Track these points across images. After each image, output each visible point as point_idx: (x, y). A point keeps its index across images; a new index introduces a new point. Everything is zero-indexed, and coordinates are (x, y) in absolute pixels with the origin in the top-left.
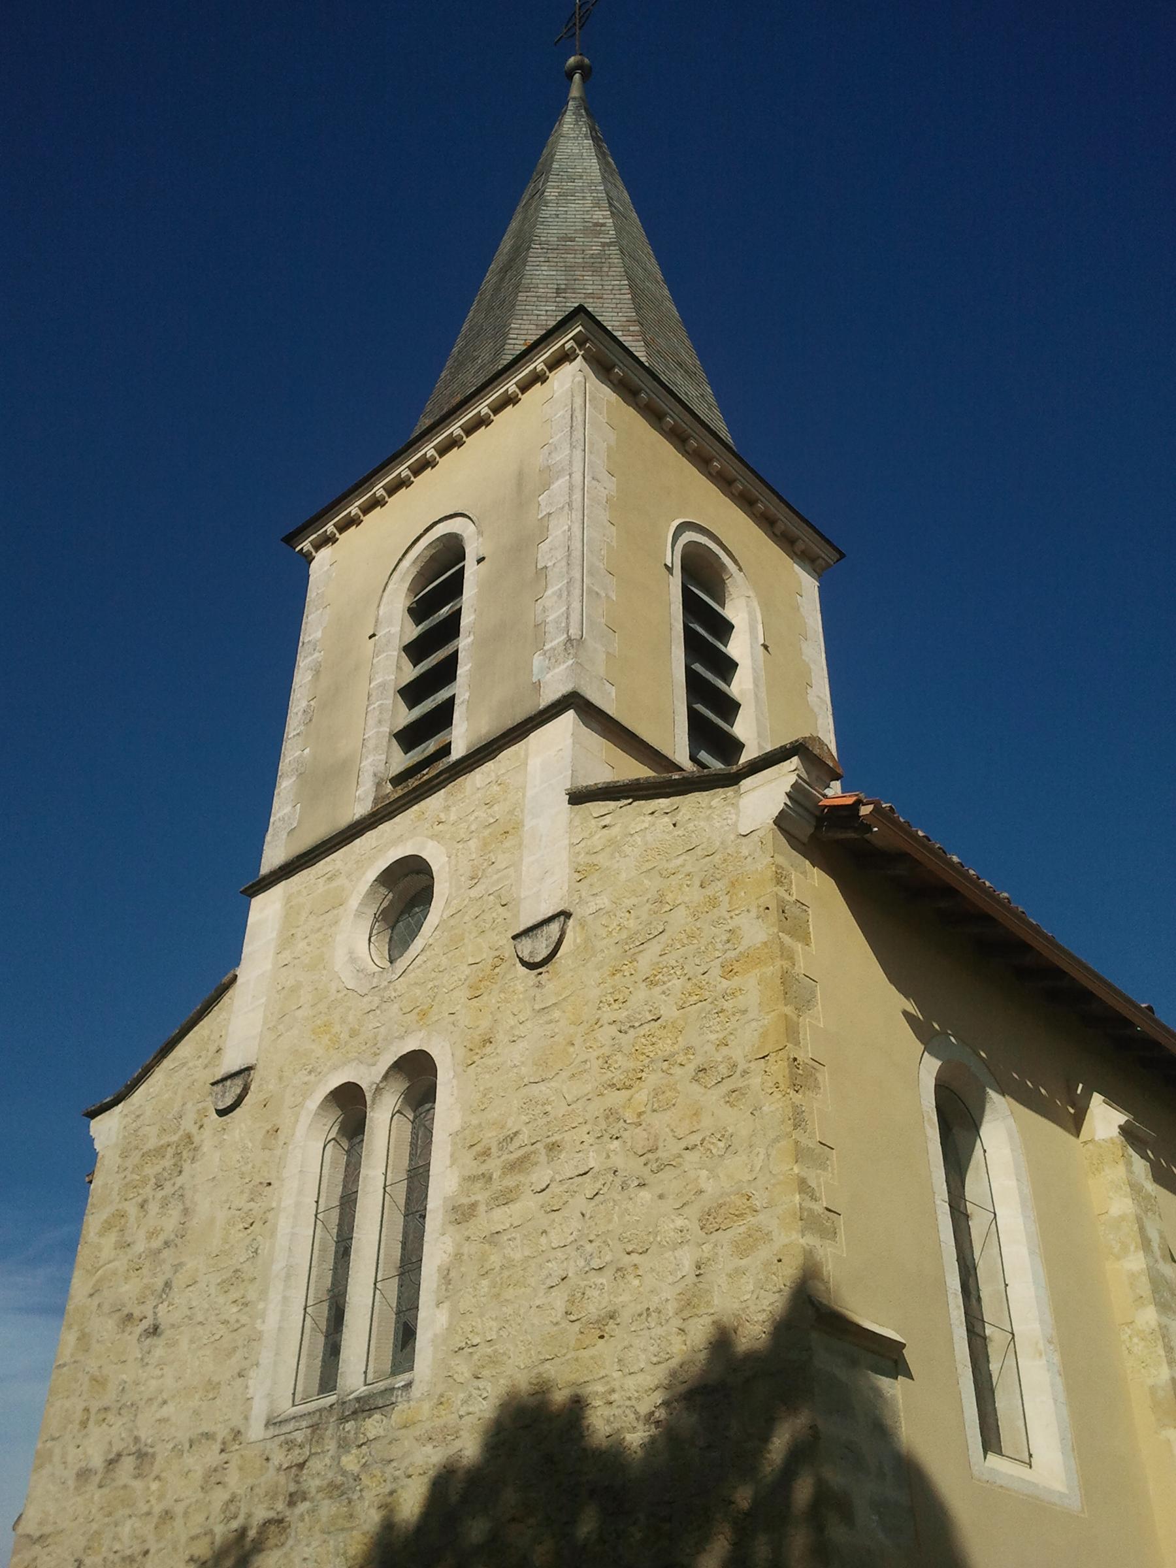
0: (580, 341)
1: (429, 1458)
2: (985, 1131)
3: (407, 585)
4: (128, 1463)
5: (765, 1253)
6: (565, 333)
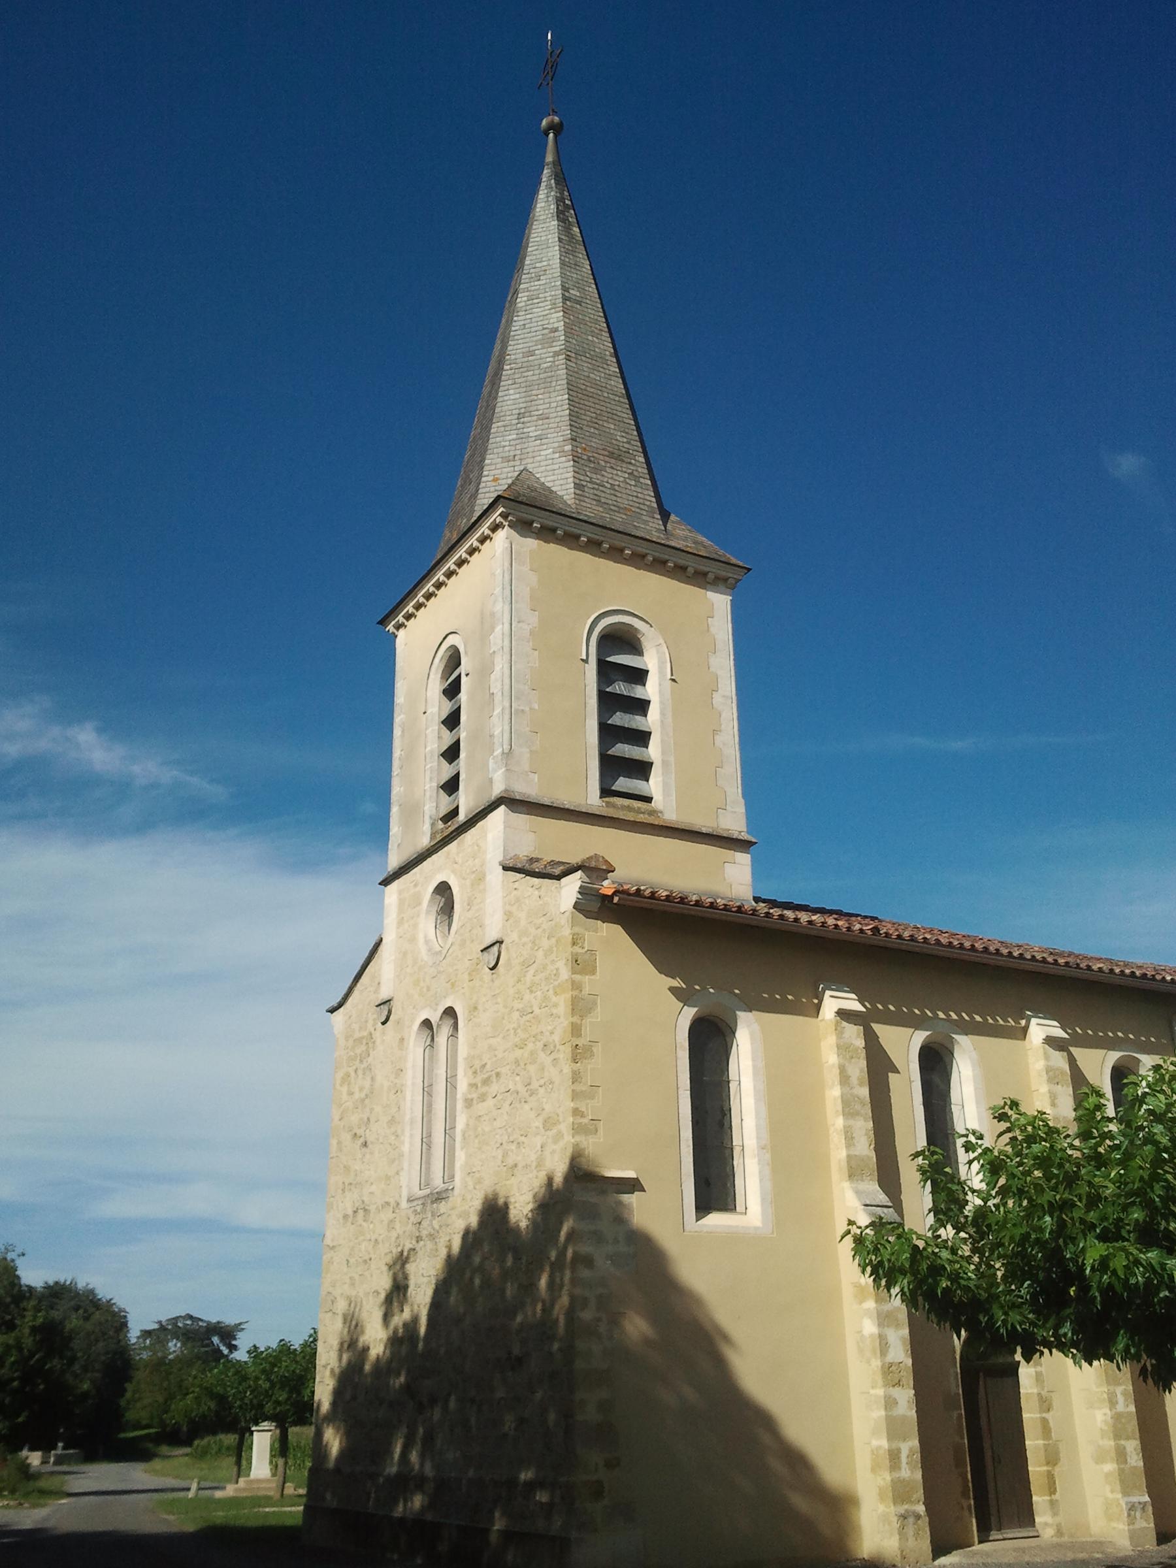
0: (504, 516)
1: (460, 1225)
2: (737, 1035)
3: (439, 675)
4: (361, 1212)
5: (561, 1144)
6: (495, 511)
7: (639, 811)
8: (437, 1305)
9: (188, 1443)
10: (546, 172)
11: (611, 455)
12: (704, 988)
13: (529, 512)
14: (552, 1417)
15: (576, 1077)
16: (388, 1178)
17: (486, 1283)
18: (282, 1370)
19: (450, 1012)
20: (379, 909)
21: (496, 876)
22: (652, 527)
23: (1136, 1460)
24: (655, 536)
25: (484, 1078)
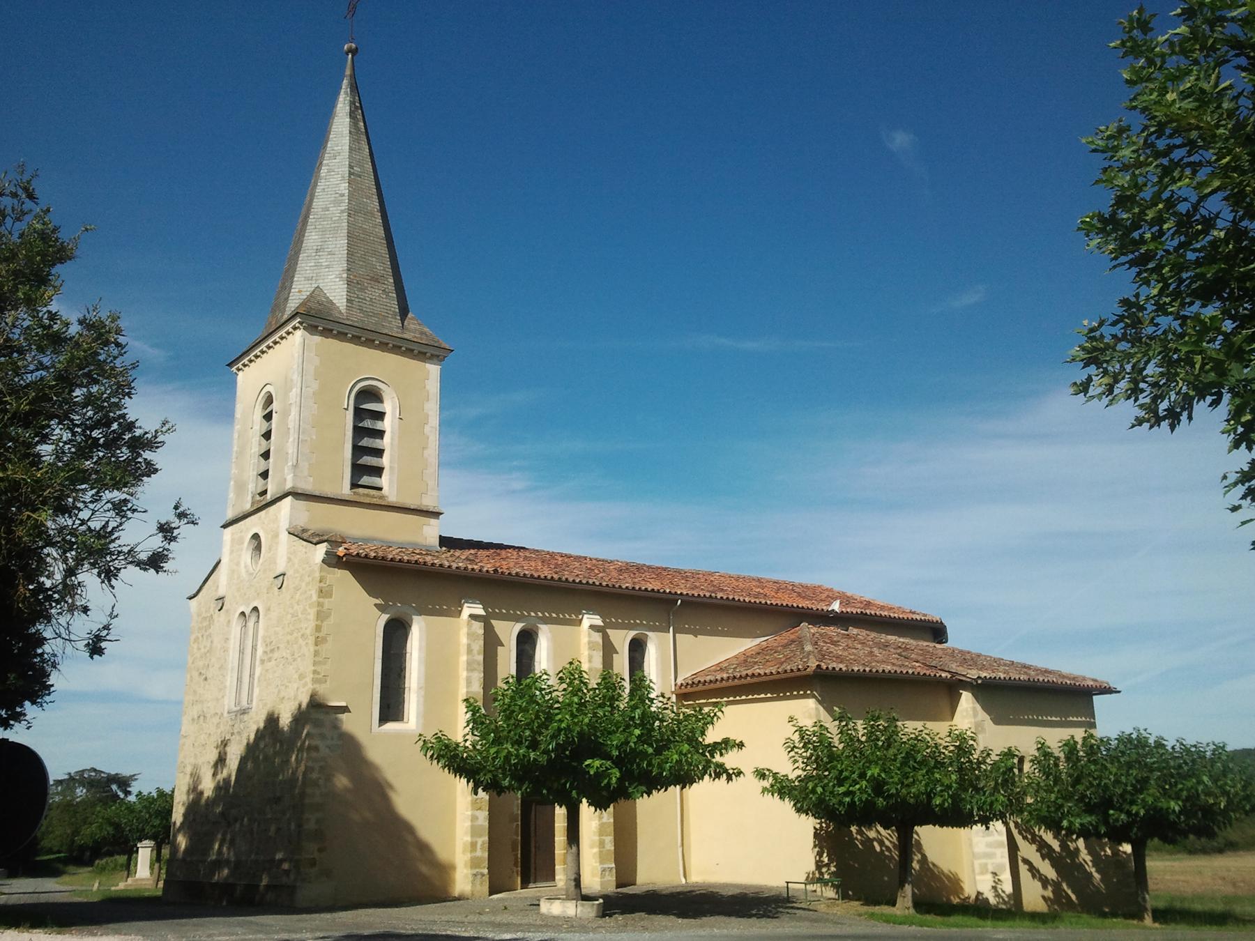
1: (254, 728)
7: (373, 497)
8: (240, 769)
9: (89, 863)
10: (345, 82)
11: (372, 279)
12: (395, 604)
13: (318, 319)
14: (293, 826)
15: (316, 653)
16: (218, 700)
17: (266, 758)
18: (156, 807)
19: (255, 609)
20: (222, 535)
21: (284, 536)
22: (392, 326)
23: (610, 846)
24: (396, 332)
25: (271, 649)
